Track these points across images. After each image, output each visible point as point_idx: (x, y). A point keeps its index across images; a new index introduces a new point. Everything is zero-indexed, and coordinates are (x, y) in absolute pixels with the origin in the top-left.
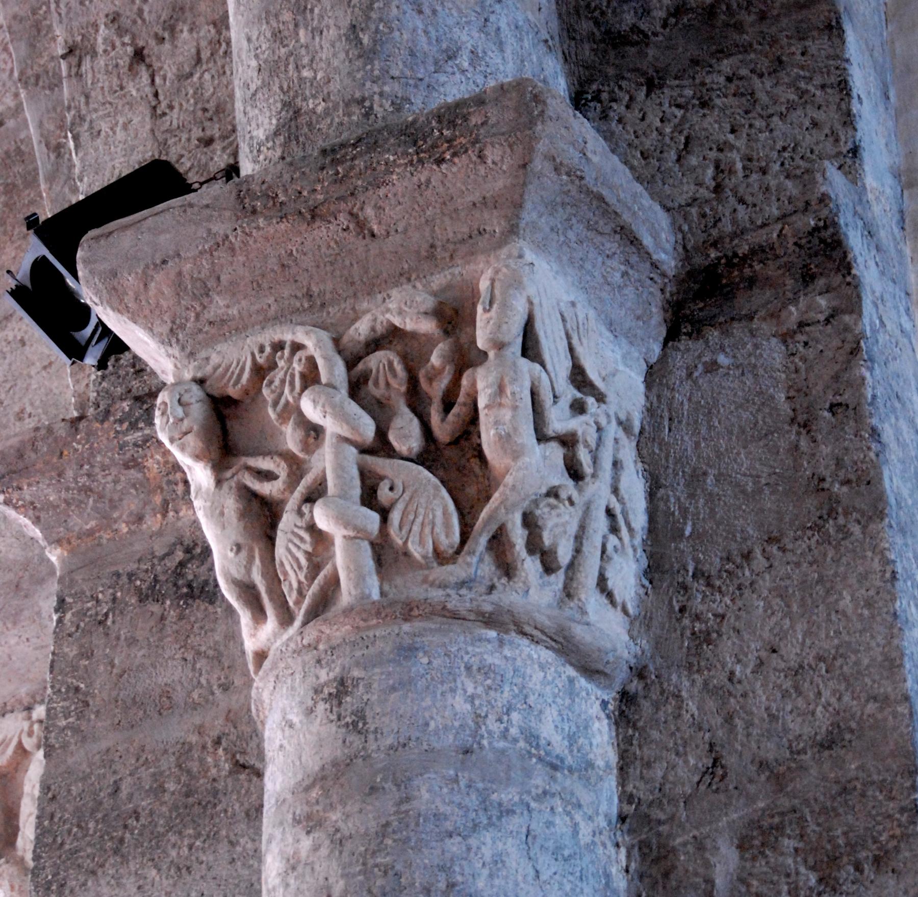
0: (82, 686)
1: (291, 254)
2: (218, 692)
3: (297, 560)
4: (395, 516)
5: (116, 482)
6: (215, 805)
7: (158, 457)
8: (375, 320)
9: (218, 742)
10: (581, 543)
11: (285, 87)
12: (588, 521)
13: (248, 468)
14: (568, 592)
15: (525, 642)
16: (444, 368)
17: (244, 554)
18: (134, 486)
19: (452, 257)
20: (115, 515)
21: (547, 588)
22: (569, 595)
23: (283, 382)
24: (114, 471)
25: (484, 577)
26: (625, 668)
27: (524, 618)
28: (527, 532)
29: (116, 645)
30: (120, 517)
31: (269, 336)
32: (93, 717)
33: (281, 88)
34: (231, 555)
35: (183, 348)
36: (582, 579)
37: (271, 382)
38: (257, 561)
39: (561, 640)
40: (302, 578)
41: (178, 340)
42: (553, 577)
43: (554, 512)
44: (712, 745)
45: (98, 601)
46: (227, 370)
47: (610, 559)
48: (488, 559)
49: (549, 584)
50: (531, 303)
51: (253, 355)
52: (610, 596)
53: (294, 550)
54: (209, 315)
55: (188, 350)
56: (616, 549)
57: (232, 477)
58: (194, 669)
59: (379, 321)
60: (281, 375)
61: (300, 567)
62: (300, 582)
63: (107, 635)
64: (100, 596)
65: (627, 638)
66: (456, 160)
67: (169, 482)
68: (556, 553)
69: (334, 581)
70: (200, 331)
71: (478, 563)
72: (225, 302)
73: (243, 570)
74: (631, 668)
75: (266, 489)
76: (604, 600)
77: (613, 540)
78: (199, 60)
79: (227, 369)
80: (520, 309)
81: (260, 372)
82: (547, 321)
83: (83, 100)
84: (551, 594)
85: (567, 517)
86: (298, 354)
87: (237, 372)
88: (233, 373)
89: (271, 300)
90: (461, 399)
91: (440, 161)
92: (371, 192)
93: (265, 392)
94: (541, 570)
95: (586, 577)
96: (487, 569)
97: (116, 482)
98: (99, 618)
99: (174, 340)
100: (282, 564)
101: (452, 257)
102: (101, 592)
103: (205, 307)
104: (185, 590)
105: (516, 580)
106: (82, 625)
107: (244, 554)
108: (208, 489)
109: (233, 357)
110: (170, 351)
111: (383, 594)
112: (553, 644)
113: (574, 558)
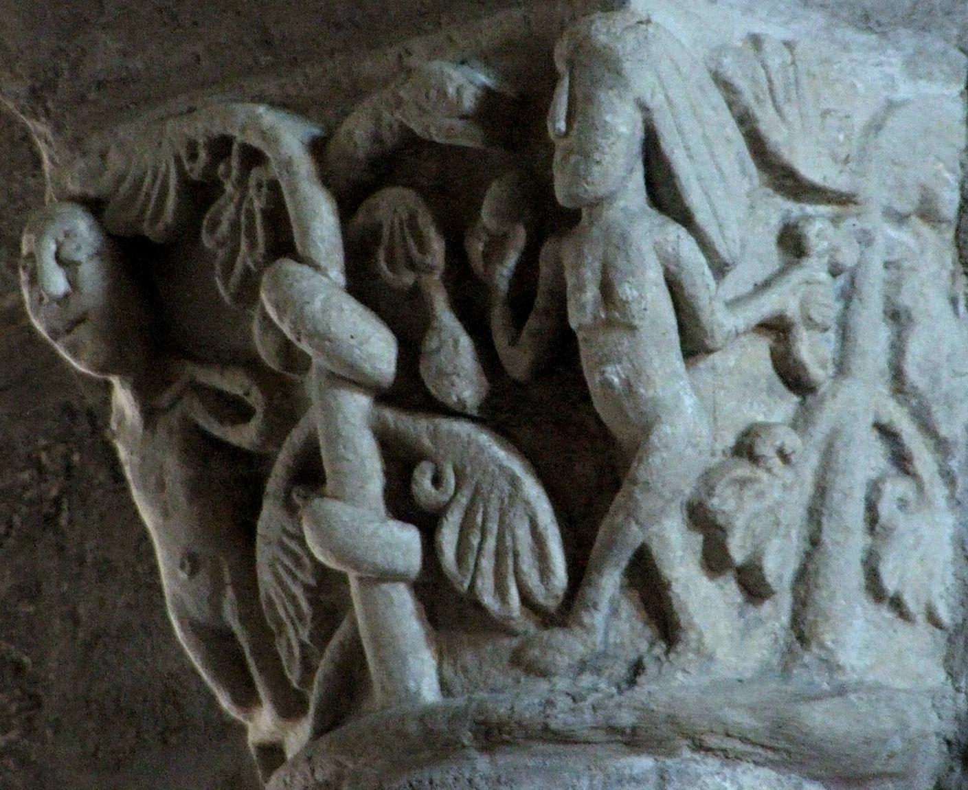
0: (26, 659)
3: (293, 599)
4: (448, 538)
8: (378, 119)
10: (819, 523)
12: (830, 476)
13: (197, 389)
14: (802, 631)
15: (713, 763)
16: (485, 266)
17: (202, 576)
21: (760, 631)
22: (802, 639)
23: (235, 226)
25: (622, 645)
26: (934, 741)
27: (703, 725)
28: (700, 538)
29: (79, 576)
32: (49, 732)
34: (183, 576)
36: (823, 604)
37: (215, 224)
38: (230, 593)
39: (782, 744)
40: (306, 639)
41: (47, 110)
42: (767, 607)
43: (748, 493)
45: (40, 469)
47: (889, 531)
48: (627, 608)
49: (760, 621)
50: (644, 108)
51: (178, 160)
52: (897, 604)
55: (69, 133)
56: (903, 504)
57: (172, 406)
59: (385, 122)
60: (229, 213)
61: (301, 618)
62: (302, 645)
63: (61, 549)
64: (44, 456)
65: (942, 675)
68: (760, 569)
70: (83, 99)
71: (611, 615)
72: (120, 45)
73: (206, 608)
74: (949, 743)
76: (887, 614)
77: (896, 488)
79: (138, 184)
80: (623, 129)
81: (200, 195)
82: (689, 124)
84: (766, 641)
85: (777, 494)
86: (256, 174)
87: (156, 191)
88: (148, 195)
90: (540, 302)
93: (207, 242)
94: (739, 599)
95: (832, 598)
96: (625, 627)
98: (46, 508)
99: (40, 110)
100: (271, 603)
102: (46, 448)
105: (680, 648)
106: (17, 520)
107: (202, 576)
111: (445, 687)
112: (770, 754)
113: (808, 555)
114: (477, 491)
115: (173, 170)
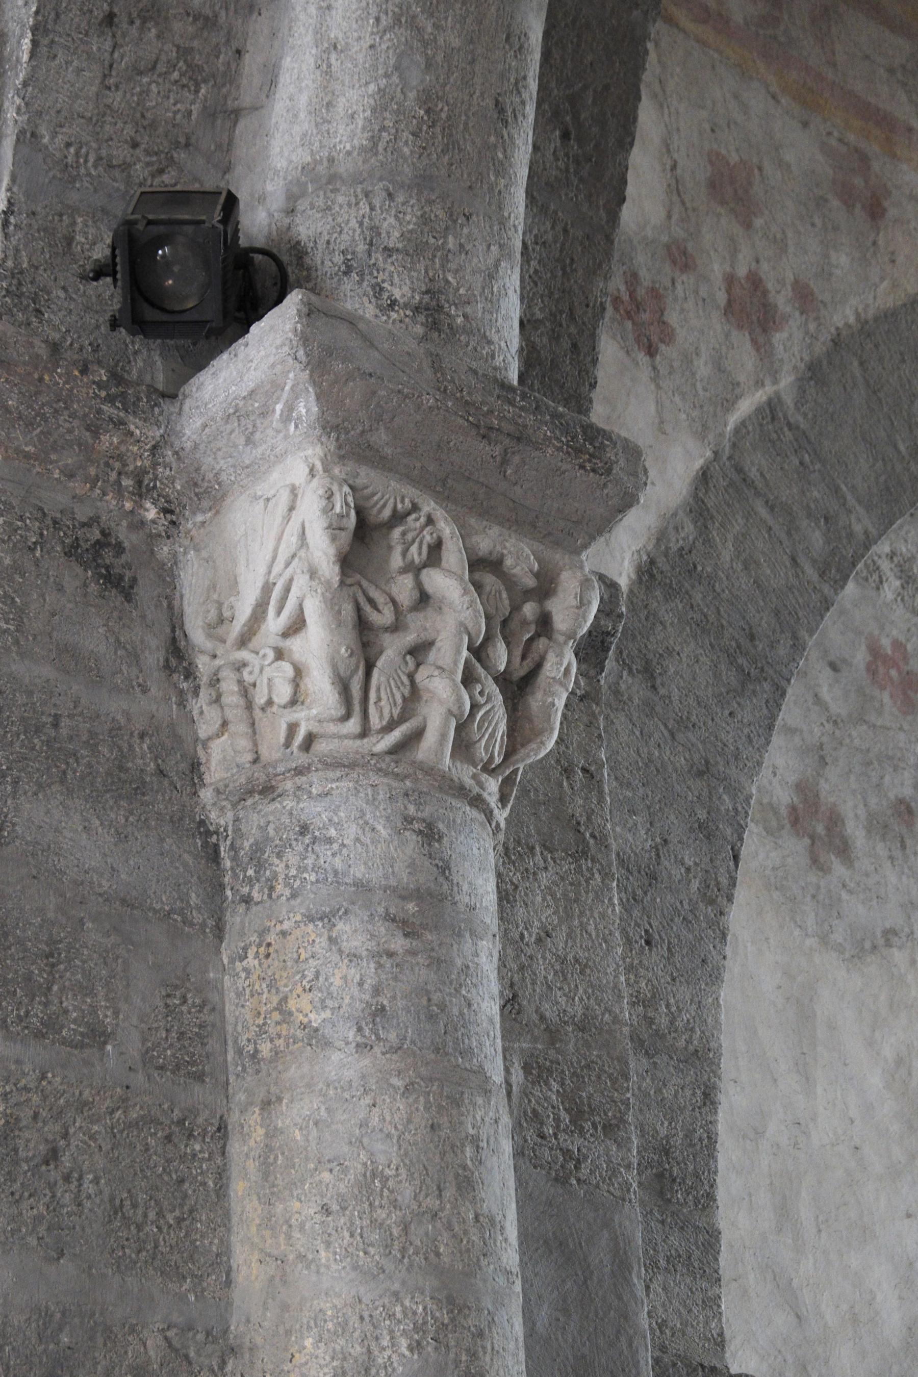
1: (448, 443)
2: (137, 689)
5: (70, 431)
6: (143, 794)
7: (115, 440)
9: (142, 736)
11: (431, 274)
13: (361, 586)
18: (80, 445)
19: (544, 537)
20: (53, 457)
24: (76, 423)
30: (56, 461)
31: (411, 492)
33: (426, 272)
35: (340, 447)
44: (512, 985)
46: (374, 494)
53: (395, 690)
54: (373, 438)
55: (343, 452)
58: (116, 653)
61: (395, 705)
66: (592, 474)
67: (107, 464)
69: (418, 735)
75: (374, 617)
78: (154, 67)
81: (398, 518)
83: (53, 15)
87: (381, 503)
88: (377, 503)
89: (418, 465)
91: (582, 467)
92: (529, 449)
97: (70, 431)
100: (378, 690)
101: (544, 537)
103: (371, 430)
104: (103, 571)
108: (328, 583)
109: (389, 493)
110: (324, 439)
114: (493, 707)
115: (392, 500)
